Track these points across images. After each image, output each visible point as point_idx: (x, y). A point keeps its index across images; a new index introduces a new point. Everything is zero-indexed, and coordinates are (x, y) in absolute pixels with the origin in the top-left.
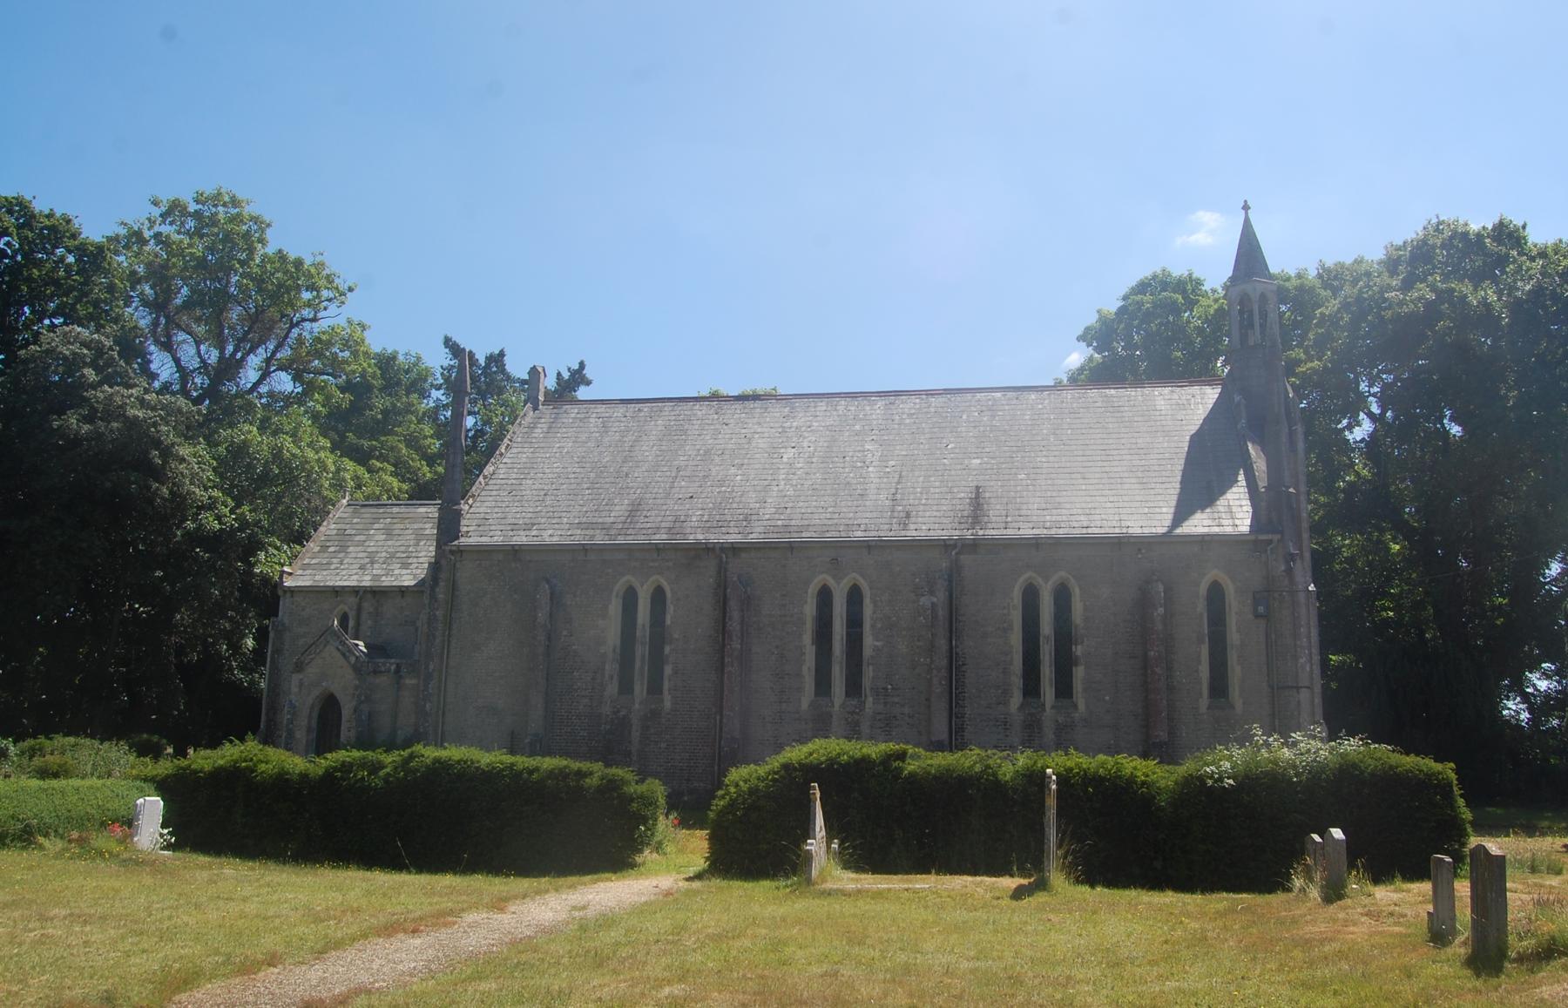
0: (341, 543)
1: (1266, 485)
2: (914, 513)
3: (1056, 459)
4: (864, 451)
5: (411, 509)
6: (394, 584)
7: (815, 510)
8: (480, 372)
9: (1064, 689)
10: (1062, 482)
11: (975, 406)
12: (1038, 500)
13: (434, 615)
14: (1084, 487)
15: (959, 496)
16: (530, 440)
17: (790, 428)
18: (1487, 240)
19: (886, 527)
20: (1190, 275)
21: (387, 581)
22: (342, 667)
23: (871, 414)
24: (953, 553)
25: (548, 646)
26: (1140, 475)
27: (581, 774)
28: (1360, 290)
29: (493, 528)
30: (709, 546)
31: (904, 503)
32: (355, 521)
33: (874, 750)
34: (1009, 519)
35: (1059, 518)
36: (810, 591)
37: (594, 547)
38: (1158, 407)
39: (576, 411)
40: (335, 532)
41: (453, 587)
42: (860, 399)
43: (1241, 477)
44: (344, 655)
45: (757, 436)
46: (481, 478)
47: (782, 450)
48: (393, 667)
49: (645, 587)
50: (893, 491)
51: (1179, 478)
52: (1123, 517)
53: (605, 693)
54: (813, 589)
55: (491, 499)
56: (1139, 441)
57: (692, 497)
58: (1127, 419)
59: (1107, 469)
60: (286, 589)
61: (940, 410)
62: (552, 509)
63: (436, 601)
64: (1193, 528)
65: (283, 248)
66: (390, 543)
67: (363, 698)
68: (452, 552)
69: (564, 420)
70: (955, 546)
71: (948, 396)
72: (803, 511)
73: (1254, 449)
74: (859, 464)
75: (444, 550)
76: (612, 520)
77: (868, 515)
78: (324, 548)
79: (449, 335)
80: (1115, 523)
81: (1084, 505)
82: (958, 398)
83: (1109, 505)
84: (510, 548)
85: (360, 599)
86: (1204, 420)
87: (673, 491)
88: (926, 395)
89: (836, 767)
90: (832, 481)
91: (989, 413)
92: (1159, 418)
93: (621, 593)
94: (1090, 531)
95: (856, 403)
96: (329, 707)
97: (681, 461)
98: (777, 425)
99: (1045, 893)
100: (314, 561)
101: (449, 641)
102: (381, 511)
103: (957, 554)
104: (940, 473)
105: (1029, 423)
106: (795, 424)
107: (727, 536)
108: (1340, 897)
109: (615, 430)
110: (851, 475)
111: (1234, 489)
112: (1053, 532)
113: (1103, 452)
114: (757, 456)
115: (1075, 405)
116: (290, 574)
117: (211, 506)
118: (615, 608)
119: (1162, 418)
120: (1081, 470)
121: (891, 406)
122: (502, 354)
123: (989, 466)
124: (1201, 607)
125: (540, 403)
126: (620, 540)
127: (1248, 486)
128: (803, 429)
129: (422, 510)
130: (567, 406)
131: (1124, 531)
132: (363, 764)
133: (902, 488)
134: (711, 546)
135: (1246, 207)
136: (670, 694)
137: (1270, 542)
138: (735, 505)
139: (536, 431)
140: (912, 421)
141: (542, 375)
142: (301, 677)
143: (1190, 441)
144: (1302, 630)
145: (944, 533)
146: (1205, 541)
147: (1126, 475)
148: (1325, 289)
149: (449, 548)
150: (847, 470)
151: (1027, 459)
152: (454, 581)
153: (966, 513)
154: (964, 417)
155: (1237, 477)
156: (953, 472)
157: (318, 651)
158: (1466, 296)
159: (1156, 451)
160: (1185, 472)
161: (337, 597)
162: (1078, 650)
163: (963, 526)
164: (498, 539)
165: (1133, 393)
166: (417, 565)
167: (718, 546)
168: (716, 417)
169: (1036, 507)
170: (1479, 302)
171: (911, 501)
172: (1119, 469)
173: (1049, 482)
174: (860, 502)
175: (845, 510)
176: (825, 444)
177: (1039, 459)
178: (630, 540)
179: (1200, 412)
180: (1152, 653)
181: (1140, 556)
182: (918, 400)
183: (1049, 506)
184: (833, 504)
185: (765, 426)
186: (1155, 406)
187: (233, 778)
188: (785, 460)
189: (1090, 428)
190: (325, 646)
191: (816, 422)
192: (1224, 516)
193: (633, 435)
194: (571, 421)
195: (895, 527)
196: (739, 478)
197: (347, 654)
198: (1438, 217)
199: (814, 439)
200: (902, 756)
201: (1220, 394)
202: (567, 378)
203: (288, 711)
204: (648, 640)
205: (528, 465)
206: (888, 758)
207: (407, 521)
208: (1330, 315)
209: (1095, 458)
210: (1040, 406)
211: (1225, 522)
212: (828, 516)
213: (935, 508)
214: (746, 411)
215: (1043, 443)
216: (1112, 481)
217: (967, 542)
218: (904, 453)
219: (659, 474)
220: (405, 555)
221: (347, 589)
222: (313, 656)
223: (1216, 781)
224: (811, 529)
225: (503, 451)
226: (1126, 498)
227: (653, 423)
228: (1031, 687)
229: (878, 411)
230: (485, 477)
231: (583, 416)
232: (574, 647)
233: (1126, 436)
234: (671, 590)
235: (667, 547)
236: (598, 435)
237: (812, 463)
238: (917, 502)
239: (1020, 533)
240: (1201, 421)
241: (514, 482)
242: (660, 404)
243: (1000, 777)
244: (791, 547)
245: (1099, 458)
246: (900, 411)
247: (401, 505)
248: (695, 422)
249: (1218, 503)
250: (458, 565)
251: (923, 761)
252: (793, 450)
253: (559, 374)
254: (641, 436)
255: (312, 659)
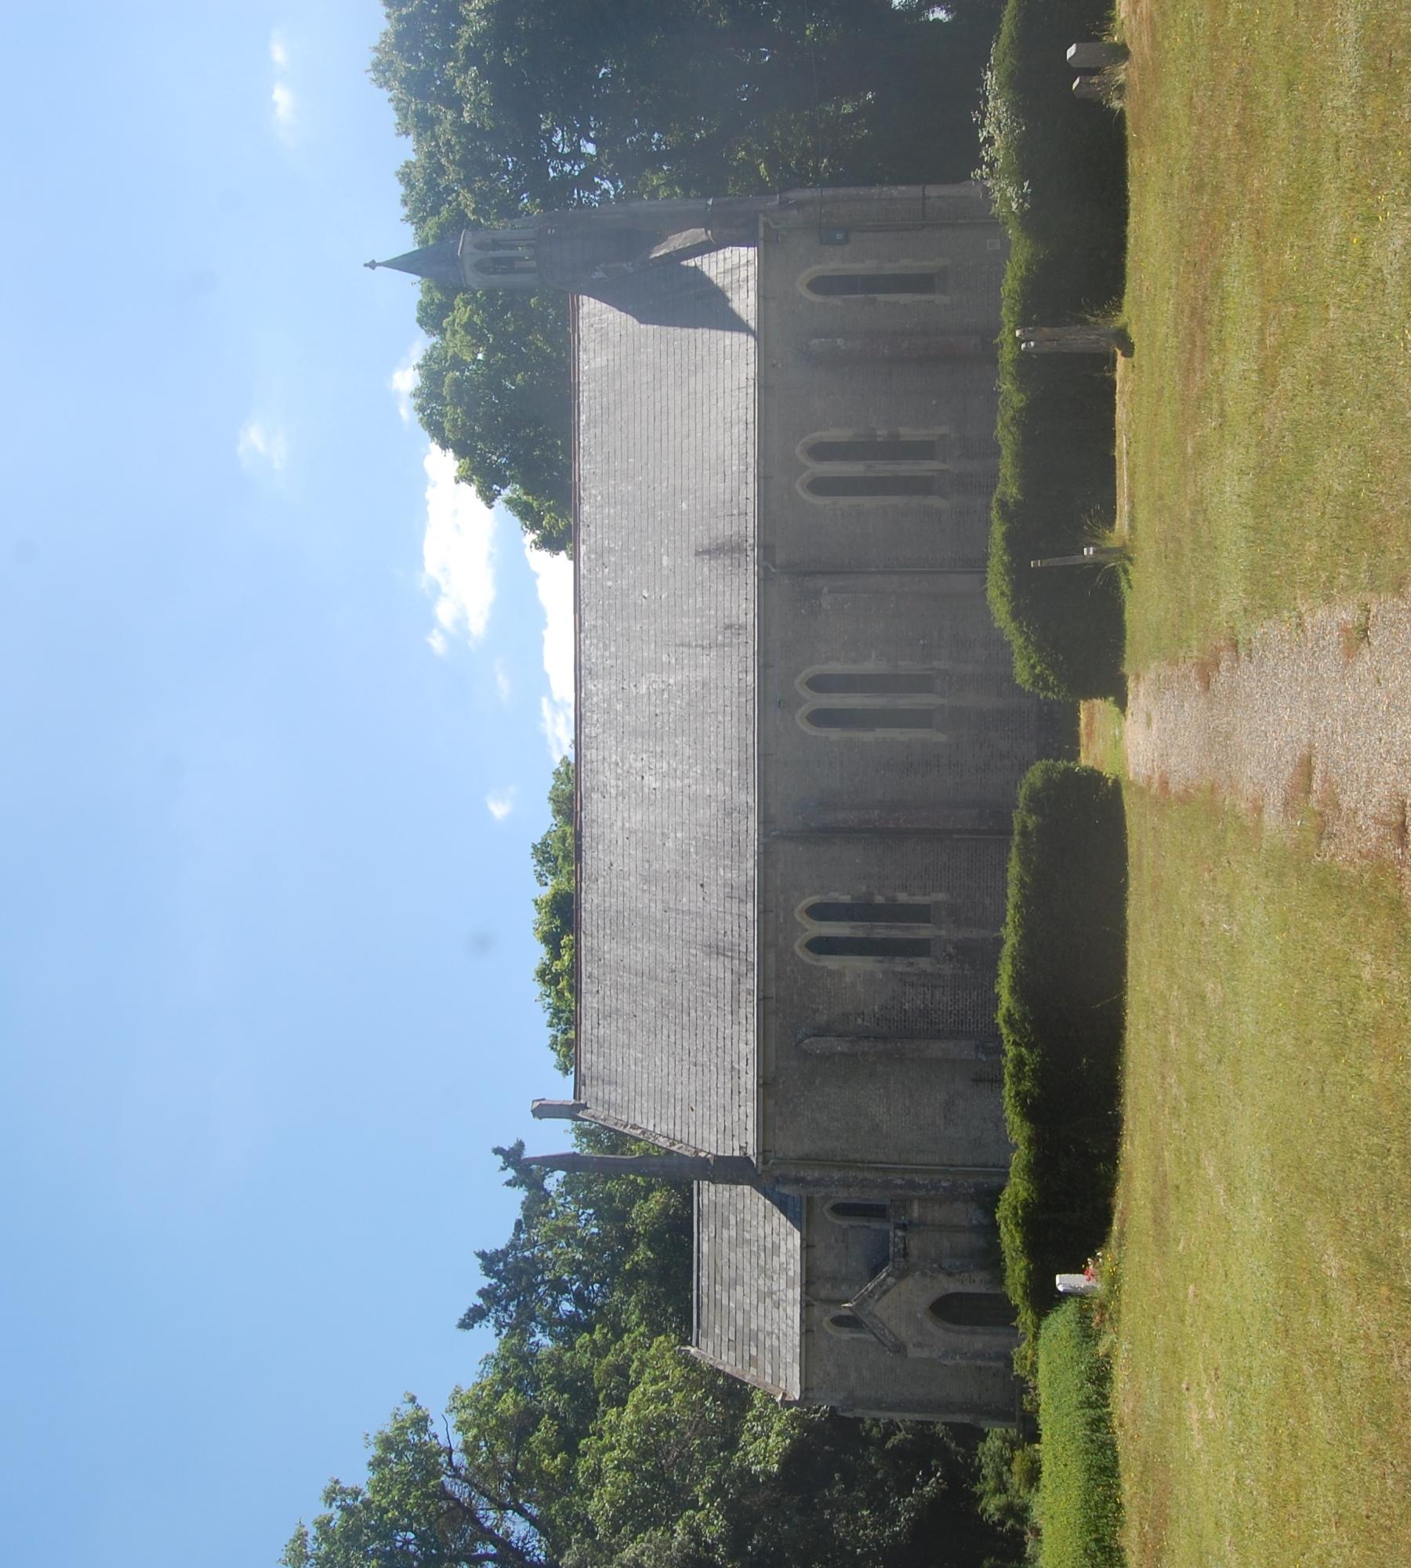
0: (746, 1341)
1: (703, 229)
2: (726, 621)
3: (664, 470)
4: (649, 694)
5: (704, 1263)
6: (798, 1257)
7: (721, 736)
8: (504, 1286)
9: (921, 914)
10: (693, 461)
11: (597, 573)
12: (713, 484)
13: (838, 1180)
14: (699, 435)
15: (707, 573)
16: (625, 1104)
17: (618, 786)
18: (404, 11)
19: (742, 649)
20: (419, 367)
21: (795, 1268)
22: (900, 1294)
23: (603, 693)
24: (773, 570)
25: (874, 1038)
26: (685, 374)
27: (1024, 833)
28: (452, 162)
29: (736, 1118)
30: (762, 850)
31: (713, 634)
32: (717, 1331)
33: (998, 530)
34: (735, 512)
35: (735, 457)
36: (813, 733)
37: (761, 988)
38: (604, 363)
39: (589, 1056)
40: (732, 1354)
41: (806, 1160)
42: (583, 710)
43: (691, 263)
44: (885, 1292)
45: (627, 825)
46: (674, 1148)
47: (646, 790)
48: (900, 1233)
49: (807, 927)
50: (699, 650)
51: (691, 331)
52: (735, 386)
53: (929, 971)
54: (812, 731)
55: (699, 1132)
56: (644, 380)
57: (702, 885)
58: (618, 398)
59: (678, 411)
60: (803, 1397)
61: (600, 613)
62: (714, 1052)
63: (823, 1179)
64: (750, 308)
65: (367, 1461)
66: (746, 1278)
67: (935, 1266)
68: (765, 1163)
69: (601, 1067)
70: (766, 569)
71: (582, 607)
72: (721, 749)
73: (658, 252)
74: (666, 696)
75: (763, 1171)
76: (728, 975)
77: (727, 673)
78: (753, 1361)
79: (457, 1322)
80: (743, 394)
81: (721, 430)
82: (585, 595)
83: (720, 404)
84: (761, 1090)
85: (816, 1300)
86: (621, 310)
87: (693, 909)
88: (580, 633)
89: (1014, 565)
90: (685, 723)
91: (606, 555)
92: (617, 362)
93: (817, 957)
94: (750, 420)
95: (588, 714)
96: (945, 1309)
97: (656, 910)
98: (614, 804)
99: (1128, 330)
100: (769, 1370)
101: (869, 1162)
102: (705, 1300)
103: (774, 567)
104: (678, 600)
105: (619, 507)
106: (613, 782)
107: (751, 832)
108: (1124, 46)
109: (615, 1001)
110: (678, 702)
111: (705, 269)
112: (751, 460)
113: (657, 419)
114: (652, 818)
115: (599, 458)
116: (784, 1395)
117: (695, 1533)
118: (831, 962)
119: (617, 358)
120: (678, 440)
121: (593, 672)
122: (482, 1255)
123: (671, 545)
124: (836, 301)
125: (578, 1102)
126: (753, 957)
127: (702, 254)
128: (619, 771)
129: (705, 1247)
130: (582, 1069)
131: (751, 382)
132: (1018, 1077)
133: (696, 640)
134: (762, 847)
135: (372, 265)
136: (929, 894)
137: (766, 225)
138: (713, 831)
139: (613, 1098)
140: (613, 644)
141: (543, 1102)
142: (911, 1346)
143: (646, 323)
144: (862, 193)
145: (750, 581)
146: (763, 296)
147: (685, 390)
148: (439, 213)
149: (760, 1165)
150: (673, 708)
151: (663, 504)
152: (799, 1159)
153: (728, 562)
154: (610, 583)
155: (691, 267)
156: (678, 585)
157: (880, 1326)
158: (475, 33)
159: (657, 360)
160: (683, 326)
161: (813, 1331)
162: (882, 433)
163: (743, 563)
164: (750, 1108)
165: (586, 394)
166: (774, 1235)
167: (761, 839)
168: (601, 880)
169: (722, 485)
170: (483, 19)
171: (712, 627)
172: (678, 399)
173: (692, 474)
174: (712, 685)
175: (721, 702)
176: (640, 740)
177: (664, 490)
178: (753, 946)
179: (611, 316)
180: (885, 351)
181: (780, 366)
182: (587, 642)
183: (721, 470)
184: (713, 716)
185: (614, 818)
186: (602, 368)
187: (1033, 1224)
188: (658, 785)
189: (627, 437)
190: (875, 1316)
191: (610, 757)
192: (735, 277)
193: (622, 977)
194: (601, 1059)
195: (742, 639)
196: (679, 835)
197: (884, 1287)
198: (367, 71)
199: (632, 756)
200: (1003, 505)
201: (589, 296)
202: (513, 1171)
203: (952, 1358)
204: (868, 923)
205: (658, 1096)
206: (1006, 514)
207: (719, 1263)
208: (476, 202)
209: (664, 427)
210: (599, 498)
211: (743, 274)
212: (728, 718)
213: (720, 598)
214: (594, 844)
215: (644, 488)
216: (692, 404)
217: (761, 555)
218: (653, 646)
219: (672, 933)
220: (763, 1254)
221: (804, 1316)
222: (886, 1331)
223: (1025, 201)
224: (743, 735)
225: (639, 1131)
226: (713, 386)
227: (607, 956)
228: (918, 948)
229: (600, 686)
230: (673, 1144)
231: (595, 1046)
232: (877, 1010)
233: (638, 396)
234: (810, 895)
235: (762, 900)
236: (620, 1021)
237: (662, 751)
238: (713, 620)
239: (752, 499)
240: (623, 313)
241: (678, 1108)
242: (583, 952)
243: (1022, 405)
244: (764, 756)
245: (665, 423)
246: (599, 660)
247: (698, 1276)
248: (607, 904)
249: (720, 285)
250: (780, 1155)
251: (1009, 488)
252: (646, 778)
253: (509, 1183)
254: (624, 967)
255: (890, 1332)
